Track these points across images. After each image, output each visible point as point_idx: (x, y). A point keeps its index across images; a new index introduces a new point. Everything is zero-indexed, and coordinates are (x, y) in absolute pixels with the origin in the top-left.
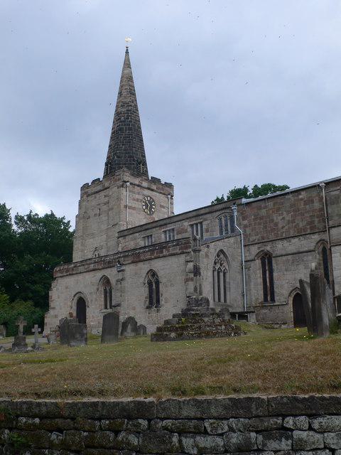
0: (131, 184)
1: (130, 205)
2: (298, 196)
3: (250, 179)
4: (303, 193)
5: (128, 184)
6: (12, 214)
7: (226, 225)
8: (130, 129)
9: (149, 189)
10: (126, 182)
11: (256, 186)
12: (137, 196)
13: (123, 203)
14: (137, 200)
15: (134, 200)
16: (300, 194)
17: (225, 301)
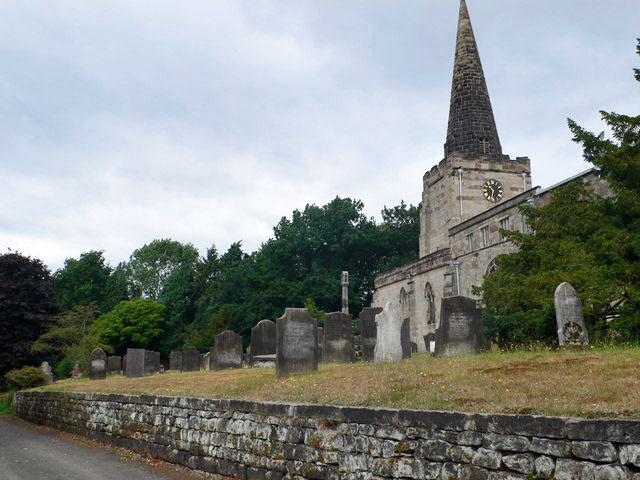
0: (465, 169)
1: (465, 195)
3: (161, 236)
5: (460, 171)
8: (469, 98)
9: (491, 170)
10: (457, 169)
11: (361, 205)
13: (455, 195)
15: (471, 187)
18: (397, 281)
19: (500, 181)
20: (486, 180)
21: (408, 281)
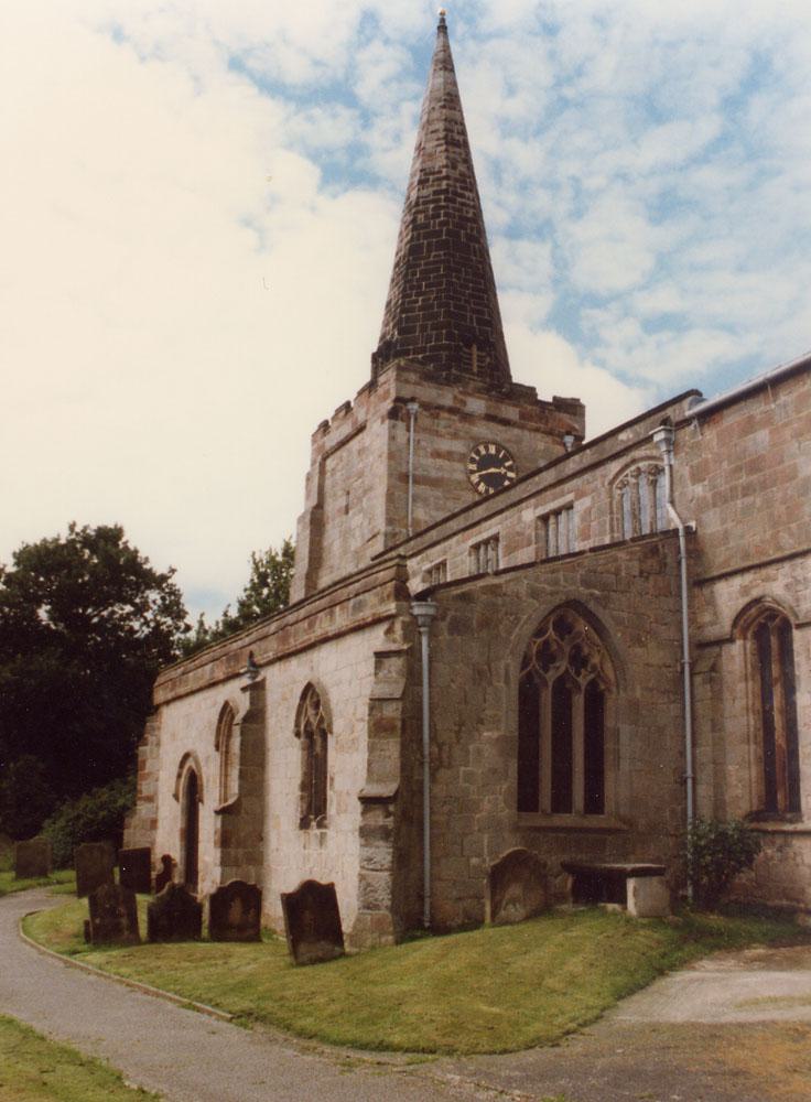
0: (425, 406)
5: (414, 407)
6: (124, 539)
7: (386, 561)
9: (490, 418)
12: (445, 445)
14: (449, 456)
15: (437, 454)
17: (595, 803)
18: (213, 684)
19: (513, 448)
20: (477, 441)
21: (246, 681)
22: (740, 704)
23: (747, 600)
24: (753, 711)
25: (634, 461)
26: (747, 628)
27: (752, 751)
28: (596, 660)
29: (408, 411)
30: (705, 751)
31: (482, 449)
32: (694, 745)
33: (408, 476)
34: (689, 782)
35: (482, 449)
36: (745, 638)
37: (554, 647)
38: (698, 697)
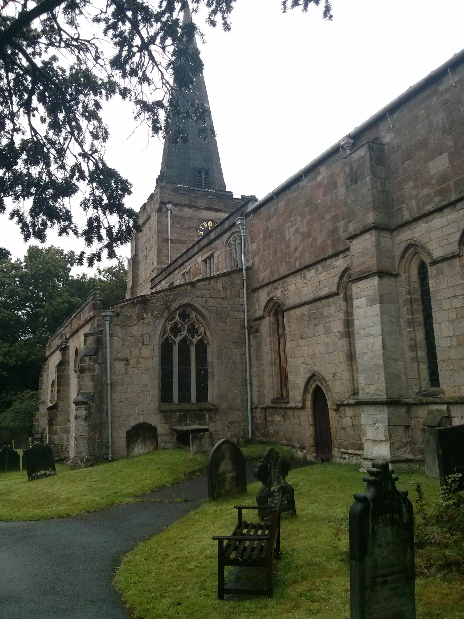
2: (315, 178)
4: (323, 170)
16: (319, 174)
22: (268, 347)
23: (268, 298)
24: (274, 351)
25: (233, 233)
26: (271, 311)
27: (273, 369)
28: (201, 330)
29: (167, 208)
30: (254, 369)
31: (205, 224)
32: (250, 367)
33: (168, 240)
34: (248, 385)
35: (205, 224)
36: (270, 317)
37: (180, 325)
38: (252, 345)
